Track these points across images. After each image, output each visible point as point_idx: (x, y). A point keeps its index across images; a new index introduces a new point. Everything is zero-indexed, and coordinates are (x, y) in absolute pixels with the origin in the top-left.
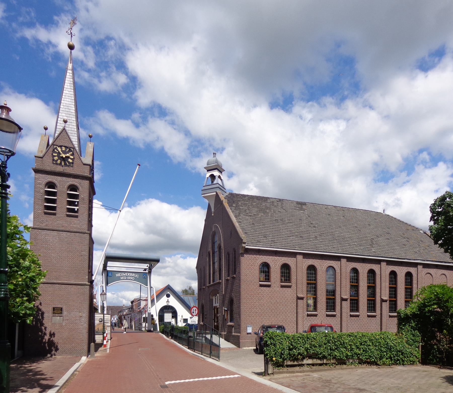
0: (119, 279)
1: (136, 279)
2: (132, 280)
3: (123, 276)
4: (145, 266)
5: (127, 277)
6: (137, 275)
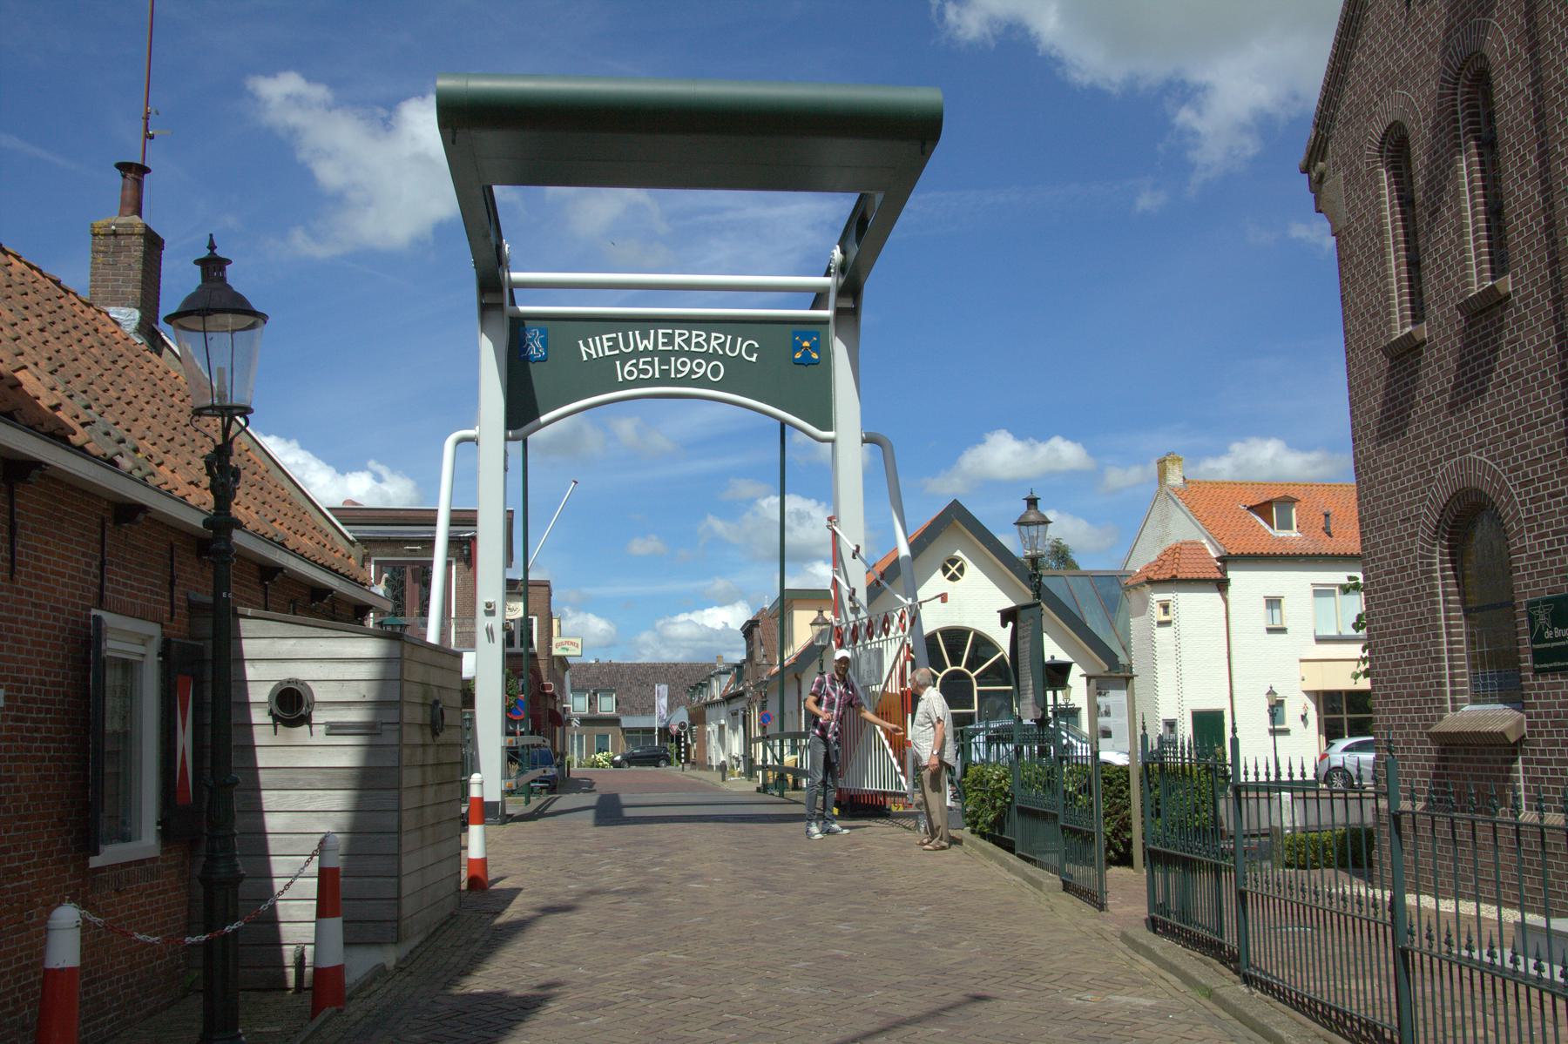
0: (601, 376)
1: (737, 377)
2: (703, 382)
3: (637, 354)
5: (665, 357)
6: (742, 347)
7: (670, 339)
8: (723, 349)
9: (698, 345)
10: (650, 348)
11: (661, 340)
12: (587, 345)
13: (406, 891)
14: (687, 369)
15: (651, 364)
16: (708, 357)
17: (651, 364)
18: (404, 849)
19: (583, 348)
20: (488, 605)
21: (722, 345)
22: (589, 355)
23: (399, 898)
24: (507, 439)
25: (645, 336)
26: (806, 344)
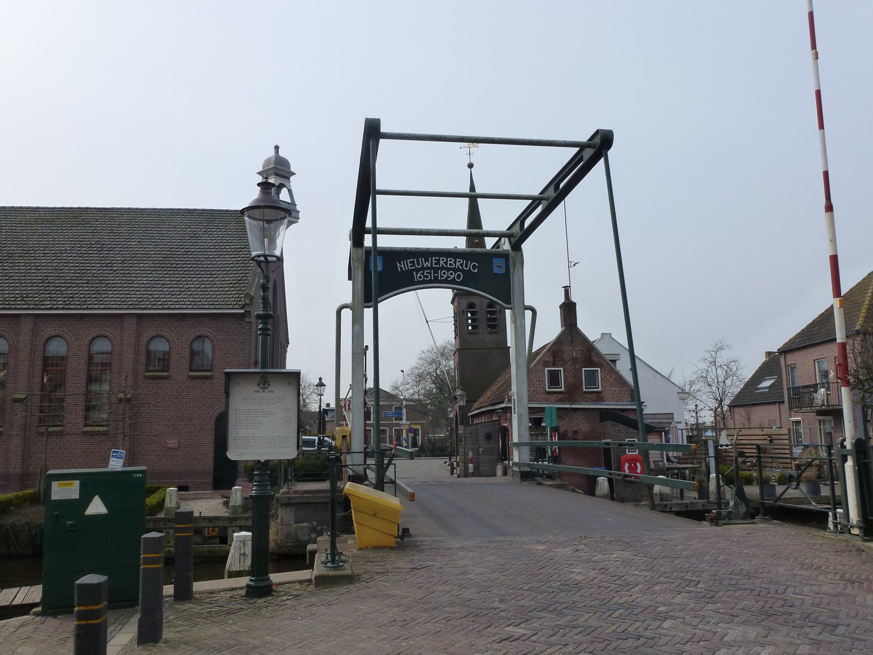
5: (436, 270)
9: (451, 264)
17: (430, 273)
22: (401, 268)
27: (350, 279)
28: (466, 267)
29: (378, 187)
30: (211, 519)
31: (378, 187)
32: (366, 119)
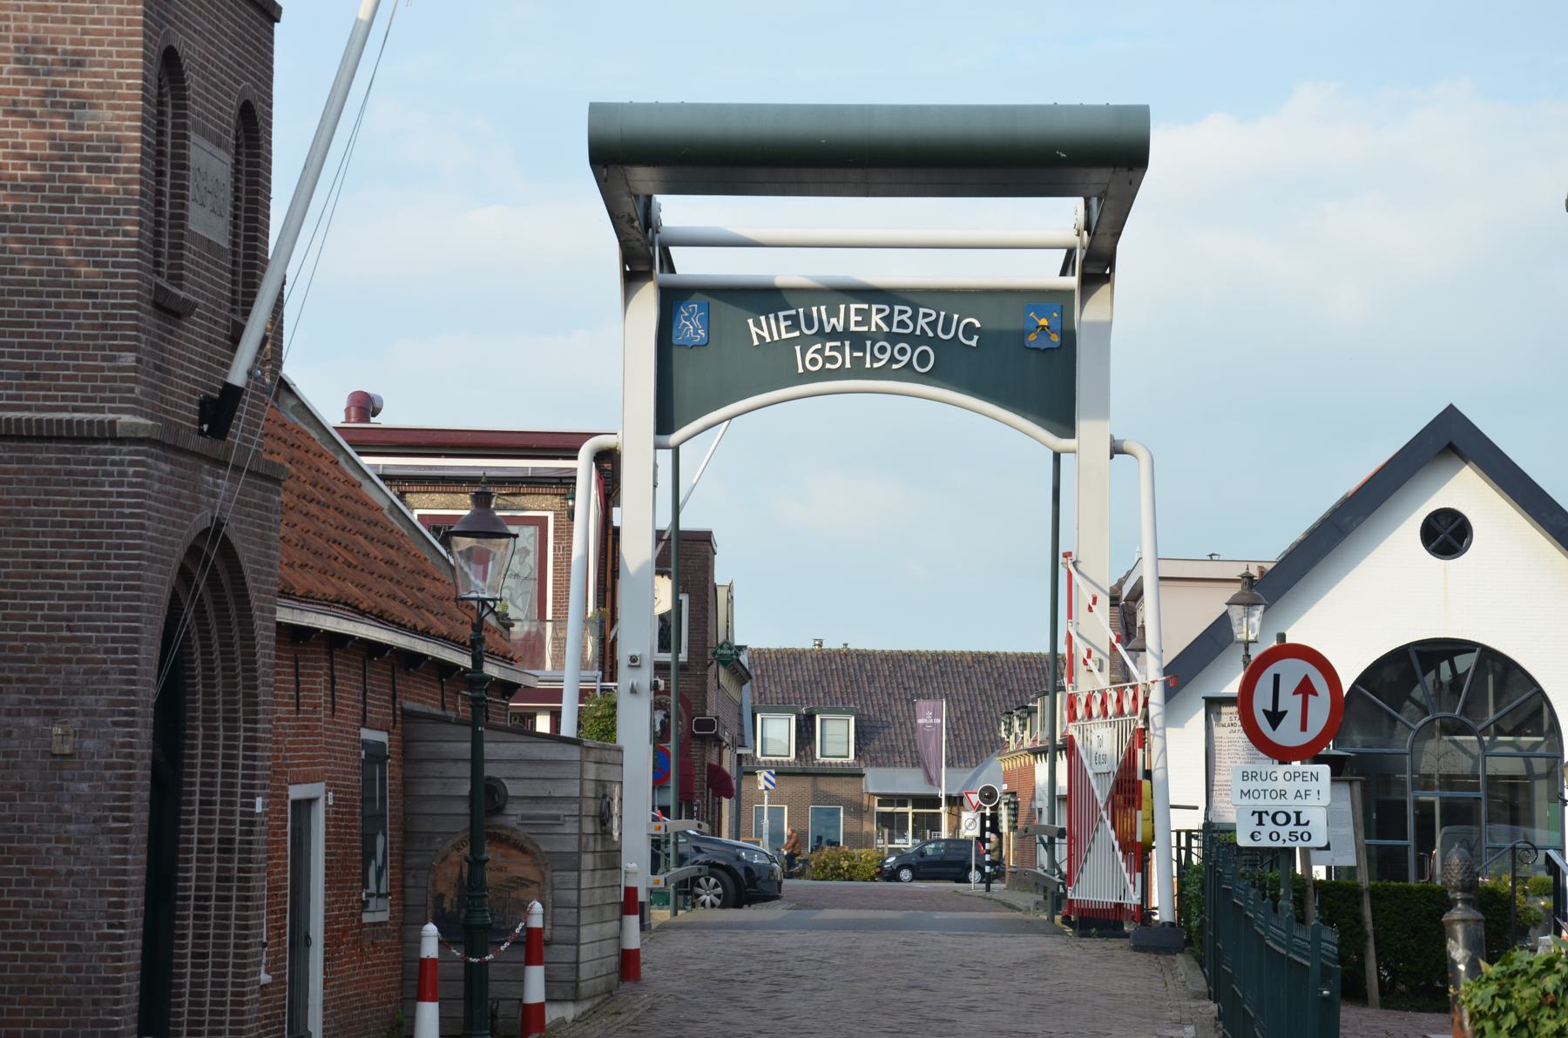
0: (775, 371)
4: (1059, 218)
5: (858, 341)
7: (865, 316)
8: (934, 330)
9: (902, 324)
10: (840, 328)
11: (853, 318)
12: (758, 325)
13: (583, 957)
14: (887, 356)
15: (841, 350)
16: (914, 340)
17: (841, 350)
18: (583, 921)
19: (753, 330)
20: (633, 659)
21: (933, 325)
22: (760, 338)
23: (577, 963)
24: (657, 447)
25: (833, 313)
26: (1044, 322)
27: (617, 531)
28: (946, 330)
29: (1045, 649)
30: (303, 409)
31: (1045, 649)
32: (1451, 410)
